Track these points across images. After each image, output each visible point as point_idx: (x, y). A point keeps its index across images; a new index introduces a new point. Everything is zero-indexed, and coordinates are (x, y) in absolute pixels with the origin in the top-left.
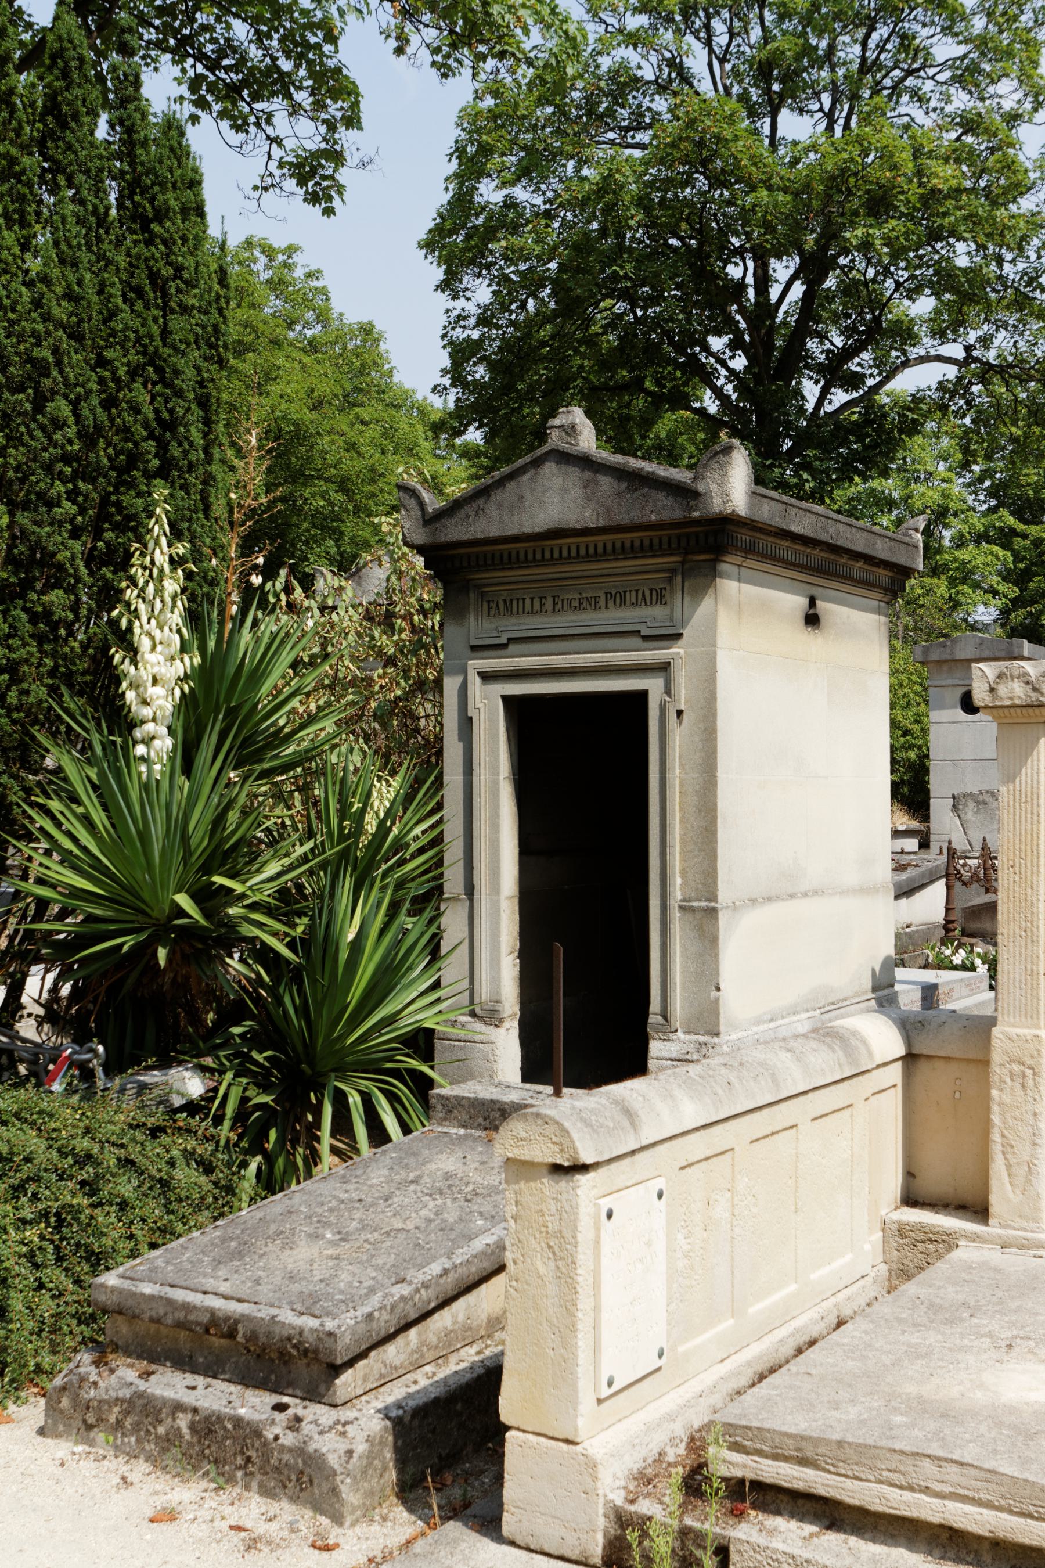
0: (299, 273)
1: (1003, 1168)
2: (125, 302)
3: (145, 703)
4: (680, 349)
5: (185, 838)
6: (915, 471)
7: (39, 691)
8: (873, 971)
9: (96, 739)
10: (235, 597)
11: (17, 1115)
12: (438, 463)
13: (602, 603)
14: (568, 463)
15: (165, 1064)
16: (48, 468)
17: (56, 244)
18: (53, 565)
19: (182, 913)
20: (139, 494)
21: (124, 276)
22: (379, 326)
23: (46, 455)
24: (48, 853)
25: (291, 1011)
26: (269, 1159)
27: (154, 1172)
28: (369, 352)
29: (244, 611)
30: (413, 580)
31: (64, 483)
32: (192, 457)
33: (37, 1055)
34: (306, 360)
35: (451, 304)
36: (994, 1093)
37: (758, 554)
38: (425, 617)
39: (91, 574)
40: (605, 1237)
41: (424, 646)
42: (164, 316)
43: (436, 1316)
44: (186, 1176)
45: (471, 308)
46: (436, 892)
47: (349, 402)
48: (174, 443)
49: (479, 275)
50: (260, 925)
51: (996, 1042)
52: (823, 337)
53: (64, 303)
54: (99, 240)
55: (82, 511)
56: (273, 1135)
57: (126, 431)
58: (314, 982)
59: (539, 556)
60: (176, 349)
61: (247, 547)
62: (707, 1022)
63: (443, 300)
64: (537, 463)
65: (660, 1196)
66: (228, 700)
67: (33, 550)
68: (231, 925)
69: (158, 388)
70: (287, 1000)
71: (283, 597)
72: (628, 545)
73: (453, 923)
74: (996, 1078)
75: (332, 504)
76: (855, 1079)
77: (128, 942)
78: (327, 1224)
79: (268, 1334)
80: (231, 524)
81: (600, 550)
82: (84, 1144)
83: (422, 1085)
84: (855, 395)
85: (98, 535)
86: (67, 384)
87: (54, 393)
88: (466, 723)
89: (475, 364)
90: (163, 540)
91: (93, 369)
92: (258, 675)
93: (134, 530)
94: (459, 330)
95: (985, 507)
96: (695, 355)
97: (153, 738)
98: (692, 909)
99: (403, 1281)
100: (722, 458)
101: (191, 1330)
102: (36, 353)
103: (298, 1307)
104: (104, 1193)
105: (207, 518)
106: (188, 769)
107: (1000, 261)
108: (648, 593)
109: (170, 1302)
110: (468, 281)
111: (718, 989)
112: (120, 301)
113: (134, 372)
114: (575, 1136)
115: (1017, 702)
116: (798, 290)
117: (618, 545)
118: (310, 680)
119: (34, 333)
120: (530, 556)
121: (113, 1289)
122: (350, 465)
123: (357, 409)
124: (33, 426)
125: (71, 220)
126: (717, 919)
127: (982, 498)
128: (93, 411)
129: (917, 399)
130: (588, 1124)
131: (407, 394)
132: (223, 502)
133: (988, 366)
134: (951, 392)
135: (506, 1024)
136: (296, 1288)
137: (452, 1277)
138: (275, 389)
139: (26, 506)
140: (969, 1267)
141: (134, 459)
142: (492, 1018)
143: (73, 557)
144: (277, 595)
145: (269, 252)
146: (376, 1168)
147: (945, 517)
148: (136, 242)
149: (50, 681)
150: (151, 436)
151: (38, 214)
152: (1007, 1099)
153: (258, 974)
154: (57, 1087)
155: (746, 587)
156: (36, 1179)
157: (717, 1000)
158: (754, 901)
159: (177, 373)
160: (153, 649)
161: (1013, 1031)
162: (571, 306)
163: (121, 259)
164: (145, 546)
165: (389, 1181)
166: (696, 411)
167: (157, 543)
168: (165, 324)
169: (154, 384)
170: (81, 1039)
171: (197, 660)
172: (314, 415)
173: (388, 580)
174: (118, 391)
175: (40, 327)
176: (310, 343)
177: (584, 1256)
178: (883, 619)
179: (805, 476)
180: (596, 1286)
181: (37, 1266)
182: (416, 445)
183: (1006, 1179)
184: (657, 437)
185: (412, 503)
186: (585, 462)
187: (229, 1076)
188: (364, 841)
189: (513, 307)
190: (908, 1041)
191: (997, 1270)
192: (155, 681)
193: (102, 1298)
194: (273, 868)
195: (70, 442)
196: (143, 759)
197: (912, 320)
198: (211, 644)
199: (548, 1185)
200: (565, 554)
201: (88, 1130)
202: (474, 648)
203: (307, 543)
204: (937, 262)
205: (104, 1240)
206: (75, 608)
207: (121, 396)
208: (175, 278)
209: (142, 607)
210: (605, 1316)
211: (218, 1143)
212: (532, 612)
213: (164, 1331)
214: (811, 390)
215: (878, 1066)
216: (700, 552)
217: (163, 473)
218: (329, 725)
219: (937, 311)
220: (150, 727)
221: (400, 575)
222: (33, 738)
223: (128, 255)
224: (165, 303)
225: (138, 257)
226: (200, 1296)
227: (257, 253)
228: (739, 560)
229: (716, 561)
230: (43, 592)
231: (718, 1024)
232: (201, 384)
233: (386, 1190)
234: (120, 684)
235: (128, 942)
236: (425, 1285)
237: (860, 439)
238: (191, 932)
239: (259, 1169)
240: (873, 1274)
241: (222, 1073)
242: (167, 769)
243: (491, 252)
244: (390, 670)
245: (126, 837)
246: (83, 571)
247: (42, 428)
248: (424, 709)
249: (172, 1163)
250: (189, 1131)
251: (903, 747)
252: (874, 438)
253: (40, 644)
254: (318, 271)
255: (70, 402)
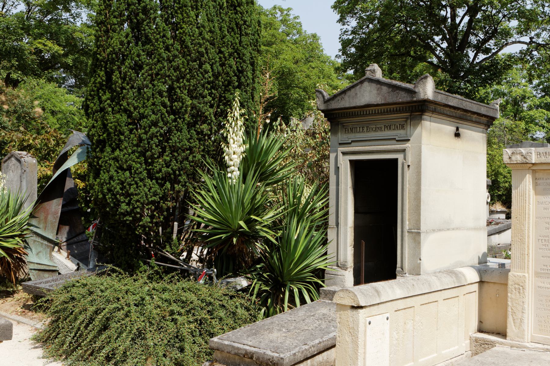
0: (291, 17)
1: (512, 320)
2: (228, 32)
3: (231, 160)
4: (424, 42)
5: (243, 204)
6: (513, 82)
7: (199, 156)
8: (479, 257)
9: (216, 172)
10: (261, 127)
11: (189, 289)
12: (339, 81)
13: (383, 129)
14: (372, 82)
15: (236, 275)
16: (203, 86)
17: (207, 15)
18: (204, 117)
19: (241, 227)
20: (231, 94)
21: (228, 24)
22: (318, 35)
23: (202, 82)
24: (201, 208)
25: (276, 261)
26: (268, 309)
27: (231, 310)
28: (315, 44)
29: (264, 132)
30: (322, 121)
31: (208, 90)
32: (248, 82)
33: (196, 272)
34: (293, 47)
35: (342, 27)
36: (509, 294)
37: (437, 112)
38: (326, 134)
39: (216, 119)
40: (368, 331)
41: (324, 143)
42: (240, 37)
43: (317, 357)
44: (241, 312)
45: (350, 28)
46: (326, 225)
47: (307, 61)
48: (242, 77)
49: (352, 17)
50: (266, 232)
51: (510, 277)
52: (477, 36)
53: (209, 34)
54: (220, 13)
55: (214, 99)
56: (269, 301)
57: (227, 73)
58: (283, 251)
59: (362, 113)
60: (244, 47)
61: (266, 110)
62: (416, 271)
63: (339, 26)
64: (362, 82)
65: (387, 319)
66: (258, 159)
67: (198, 112)
68: (257, 232)
69: (238, 60)
70: (275, 257)
71: (279, 127)
72: (392, 109)
73: (331, 234)
74: (510, 290)
75: (301, 96)
76: (460, 288)
77: (224, 236)
78: (284, 327)
79: (263, 358)
80: (261, 103)
81: (382, 111)
82: (208, 299)
83: (318, 287)
84: (488, 56)
85: (218, 107)
86: (209, 59)
87: (205, 62)
88: (337, 169)
89: (350, 47)
90: (238, 109)
91: (218, 54)
92: (268, 152)
93: (230, 105)
94: (345, 36)
95: (540, 95)
96: (428, 43)
97: (233, 171)
98: (412, 233)
99: (306, 344)
100: (424, 80)
101: (239, 356)
102: (200, 50)
103: (273, 350)
104: (215, 315)
105: (253, 101)
106: (244, 182)
107: (543, 6)
108: (398, 126)
109: (233, 347)
110: (348, 19)
111: (420, 260)
112: (226, 32)
113: (231, 55)
114: (358, 297)
115: (519, 162)
116: (467, 19)
117: (389, 110)
118: (286, 153)
119: (199, 43)
120: (359, 113)
121: (216, 342)
122: (307, 82)
123: (310, 63)
124: (199, 72)
125: (212, 7)
126: (420, 236)
127: (539, 92)
128: (217, 68)
129: (510, 57)
130: (363, 293)
131: (328, 58)
132: (259, 96)
133: (539, 45)
134: (525, 54)
135: (349, 270)
136: (272, 344)
137: (322, 344)
138: (281, 57)
139: (196, 98)
140: (498, 352)
141: (230, 83)
142: (344, 267)
143: (210, 114)
144: (277, 126)
145: (281, 10)
146: (301, 311)
147: (524, 99)
148: (232, 13)
149: (202, 153)
150: (236, 75)
151: (202, 5)
152: (513, 297)
153: (265, 248)
154: (202, 282)
155: (433, 124)
156: (194, 309)
157: (420, 263)
158: (434, 230)
159: (244, 55)
160: (234, 143)
161: (516, 274)
162: (384, 27)
163: (227, 19)
164: (232, 110)
165: (305, 315)
166: (429, 62)
167: (236, 109)
168: (241, 39)
169: (237, 58)
170: (209, 267)
171: (248, 146)
172: (295, 66)
173: (314, 121)
174: (225, 61)
175: (201, 41)
176: (295, 41)
177: (361, 336)
178: (484, 135)
179: (468, 85)
180: (365, 345)
181: (193, 336)
182: (331, 75)
183: (513, 324)
184: (416, 71)
185: (320, 96)
186: (378, 82)
187: (256, 280)
188: (301, 206)
189: (364, 27)
190: (481, 277)
191: (507, 354)
192: (234, 153)
193: (213, 345)
194: (271, 214)
195: (210, 77)
196: (230, 178)
197: (510, 28)
198: (253, 142)
199: (350, 312)
200: (371, 112)
201: (210, 295)
202: (340, 144)
203: (292, 109)
204: (519, 7)
205: (214, 330)
206: (211, 130)
207: (226, 62)
208: (244, 24)
209: (231, 129)
210: (367, 355)
211: (251, 302)
212: (360, 132)
213: (231, 356)
214: (471, 54)
215: (469, 284)
216: (416, 112)
217: (239, 87)
218: (292, 168)
219: (520, 26)
220: (232, 168)
221: (318, 120)
222: (197, 171)
223: (229, 17)
224: (241, 33)
225: (232, 18)
226: (242, 345)
227: (277, 11)
228: (430, 114)
229: (422, 115)
230: (201, 125)
231: (420, 272)
232: (252, 58)
233: (303, 318)
234: (224, 153)
235: (224, 236)
236: (313, 346)
237: (489, 72)
238: (244, 234)
239: (265, 311)
240: (466, 354)
241: (253, 279)
242: (238, 181)
243: (356, 9)
244: (314, 151)
245: (223, 202)
246: (213, 118)
247: (202, 73)
248: (325, 165)
249: (237, 307)
250: (242, 297)
251: (503, 182)
252: (495, 71)
253: (199, 141)
254: (298, 16)
255: (210, 65)
